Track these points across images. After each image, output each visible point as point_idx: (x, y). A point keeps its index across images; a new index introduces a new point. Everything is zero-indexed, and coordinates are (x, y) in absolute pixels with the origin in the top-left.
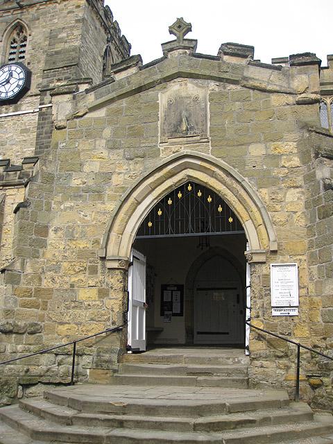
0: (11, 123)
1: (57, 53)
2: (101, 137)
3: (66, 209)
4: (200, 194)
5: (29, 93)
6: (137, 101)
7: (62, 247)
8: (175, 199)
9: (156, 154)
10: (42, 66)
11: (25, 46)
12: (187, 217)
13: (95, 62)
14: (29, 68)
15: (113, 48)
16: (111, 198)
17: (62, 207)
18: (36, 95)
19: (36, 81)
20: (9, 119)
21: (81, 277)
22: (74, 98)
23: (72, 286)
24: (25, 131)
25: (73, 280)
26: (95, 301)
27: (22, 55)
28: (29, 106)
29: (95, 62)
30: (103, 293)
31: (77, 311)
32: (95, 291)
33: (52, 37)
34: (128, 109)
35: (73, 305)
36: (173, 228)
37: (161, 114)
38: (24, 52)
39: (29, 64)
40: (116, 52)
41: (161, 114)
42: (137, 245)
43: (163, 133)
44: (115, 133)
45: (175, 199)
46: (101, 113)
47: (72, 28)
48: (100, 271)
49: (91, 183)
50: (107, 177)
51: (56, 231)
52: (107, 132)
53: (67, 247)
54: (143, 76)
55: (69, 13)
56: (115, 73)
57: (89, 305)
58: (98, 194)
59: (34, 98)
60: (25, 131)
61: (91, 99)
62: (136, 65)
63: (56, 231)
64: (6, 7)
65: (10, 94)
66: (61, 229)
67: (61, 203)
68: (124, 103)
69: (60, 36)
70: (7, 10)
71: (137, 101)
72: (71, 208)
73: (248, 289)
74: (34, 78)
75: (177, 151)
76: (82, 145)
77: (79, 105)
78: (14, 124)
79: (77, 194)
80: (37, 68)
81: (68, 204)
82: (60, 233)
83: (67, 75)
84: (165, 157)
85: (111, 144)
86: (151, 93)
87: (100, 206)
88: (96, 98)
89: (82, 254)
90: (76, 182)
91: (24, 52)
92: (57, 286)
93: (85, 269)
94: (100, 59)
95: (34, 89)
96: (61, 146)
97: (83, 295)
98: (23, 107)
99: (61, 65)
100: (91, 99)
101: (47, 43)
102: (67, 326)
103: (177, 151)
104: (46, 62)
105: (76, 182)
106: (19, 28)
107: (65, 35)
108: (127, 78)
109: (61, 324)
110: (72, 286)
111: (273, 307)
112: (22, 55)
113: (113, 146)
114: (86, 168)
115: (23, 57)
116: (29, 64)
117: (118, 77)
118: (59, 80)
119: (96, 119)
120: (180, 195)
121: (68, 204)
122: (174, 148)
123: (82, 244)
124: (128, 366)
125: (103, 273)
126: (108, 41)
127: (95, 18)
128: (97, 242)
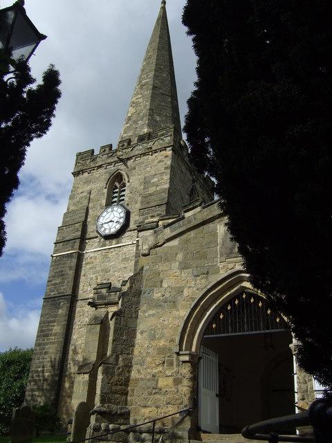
0: (114, 254)
1: (150, 195)
2: (175, 260)
3: (149, 316)
4: (252, 300)
5: (129, 229)
6: (202, 232)
7: (146, 345)
8: (233, 306)
9: (217, 271)
10: (138, 206)
11: (124, 190)
12: (243, 319)
13: (182, 199)
14: (128, 208)
15: (198, 187)
16: (184, 307)
17: (147, 314)
18: (134, 230)
19: (134, 218)
20: (112, 250)
21: (160, 368)
22: (155, 232)
23: (154, 376)
24: (126, 259)
25: (154, 371)
26: (171, 388)
27: (122, 198)
28: (128, 239)
29: (182, 199)
30: (177, 382)
31: (157, 396)
32: (171, 380)
33: (146, 182)
34: (195, 238)
35: (154, 391)
36: (232, 328)
37: (219, 241)
38: (124, 195)
39: (128, 205)
40: (201, 190)
41: (219, 241)
42: (203, 342)
43: (222, 255)
44: (185, 257)
45: (233, 306)
46: (175, 242)
47: (162, 174)
48: (175, 364)
49: (167, 295)
50: (180, 291)
51: (142, 333)
52: (180, 257)
53: (150, 346)
54: (205, 213)
55: (158, 162)
56: (185, 212)
57: (166, 391)
58: (174, 304)
59: (132, 232)
60: (126, 259)
61: (168, 233)
62: (200, 205)
63: (142, 333)
64: (109, 161)
65: (113, 231)
66: (146, 332)
67: (145, 312)
68: (192, 234)
69: (152, 181)
70: (110, 164)
71: (202, 232)
72: (153, 315)
73: (295, 376)
74: (132, 215)
75: (233, 268)
76: (161, 267)
77: (159, 237)
78: (117, 254)
79: (158, 305)
80: (135, 208)
81: (151, 312)
82: (145, 335)
83: (159, 212)
84: (223, 274)
85: (183, 266)
86: (211, 225)
87: (175, 313)
88: (171, 232)
89: (161, 351)
90: (157, 295)
91: (124, 195)
92: (142, 376)
93: (164, 362)
94: (187, 197)
95: (132, 225)
96: (145, 268)
97: (162, 383)
98: (123, 240)
99: (153, 204)
100: (168, 233)
101: (142, 187)
102: (150, 409)
103: (233, 268)
104: (142, 203)
105: (157, 295)
106: (118, 177)
107: (156, 180)
108: (194, 215)
109: (145, 407)
110: (154, 376)
111: (316, 391)
112: (122, 198)
113: (184, 266)
114: (165, 285)
115: (123, 200)
116: (128, 205)
117: (187, 215)
118: (152, 217)
119: (168, 247)
120: (237, 302)
121: (151, 312)
122: (230, 266)
123: (162, 343)
124: (72, 250)
125: (178, 365)
126: (194, 181)
127: (181, 164)
128: (172, 341)
